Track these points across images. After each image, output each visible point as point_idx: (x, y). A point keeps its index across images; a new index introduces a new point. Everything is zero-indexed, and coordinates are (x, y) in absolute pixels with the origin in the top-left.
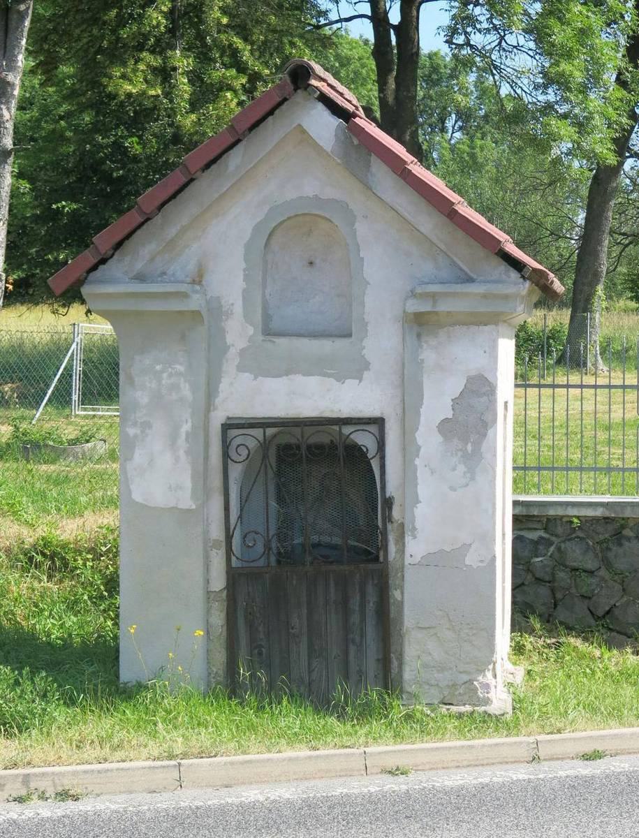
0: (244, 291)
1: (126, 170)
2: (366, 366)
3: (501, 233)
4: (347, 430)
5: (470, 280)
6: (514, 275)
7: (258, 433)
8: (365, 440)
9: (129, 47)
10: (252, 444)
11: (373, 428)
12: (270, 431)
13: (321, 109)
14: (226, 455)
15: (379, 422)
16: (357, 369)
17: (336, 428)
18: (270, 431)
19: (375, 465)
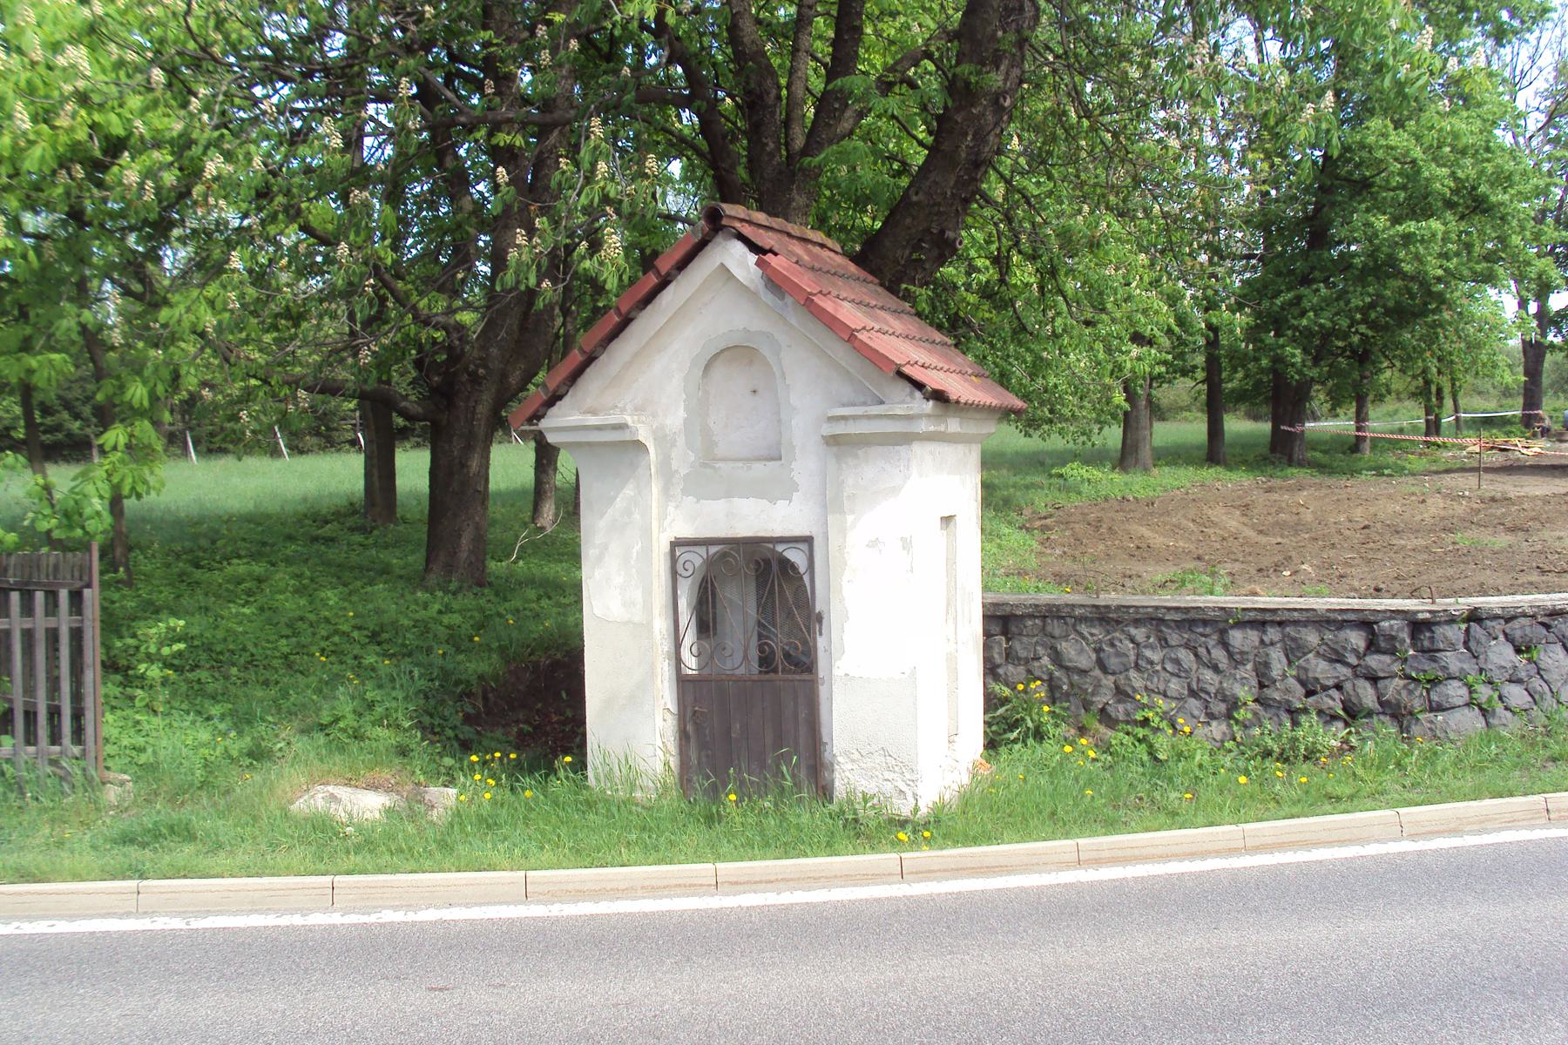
0: (685, 420)
1: (633, 105)
2: (795, 487)
3: (1408, 601)
4: (780, 548)
5: (882, 403)
6: (918, 394)
7: (702, 550)
8: (796, 556)
9: (1450, 205)
10: (698, 561)
11: (804, 547)
12: (713, 549)
13: (738, 248)
14: (674, 574)
15: (808, 540)
16: (787, 491)
17: (771, 546)
18: (713, 549)
19: (806, 579)
